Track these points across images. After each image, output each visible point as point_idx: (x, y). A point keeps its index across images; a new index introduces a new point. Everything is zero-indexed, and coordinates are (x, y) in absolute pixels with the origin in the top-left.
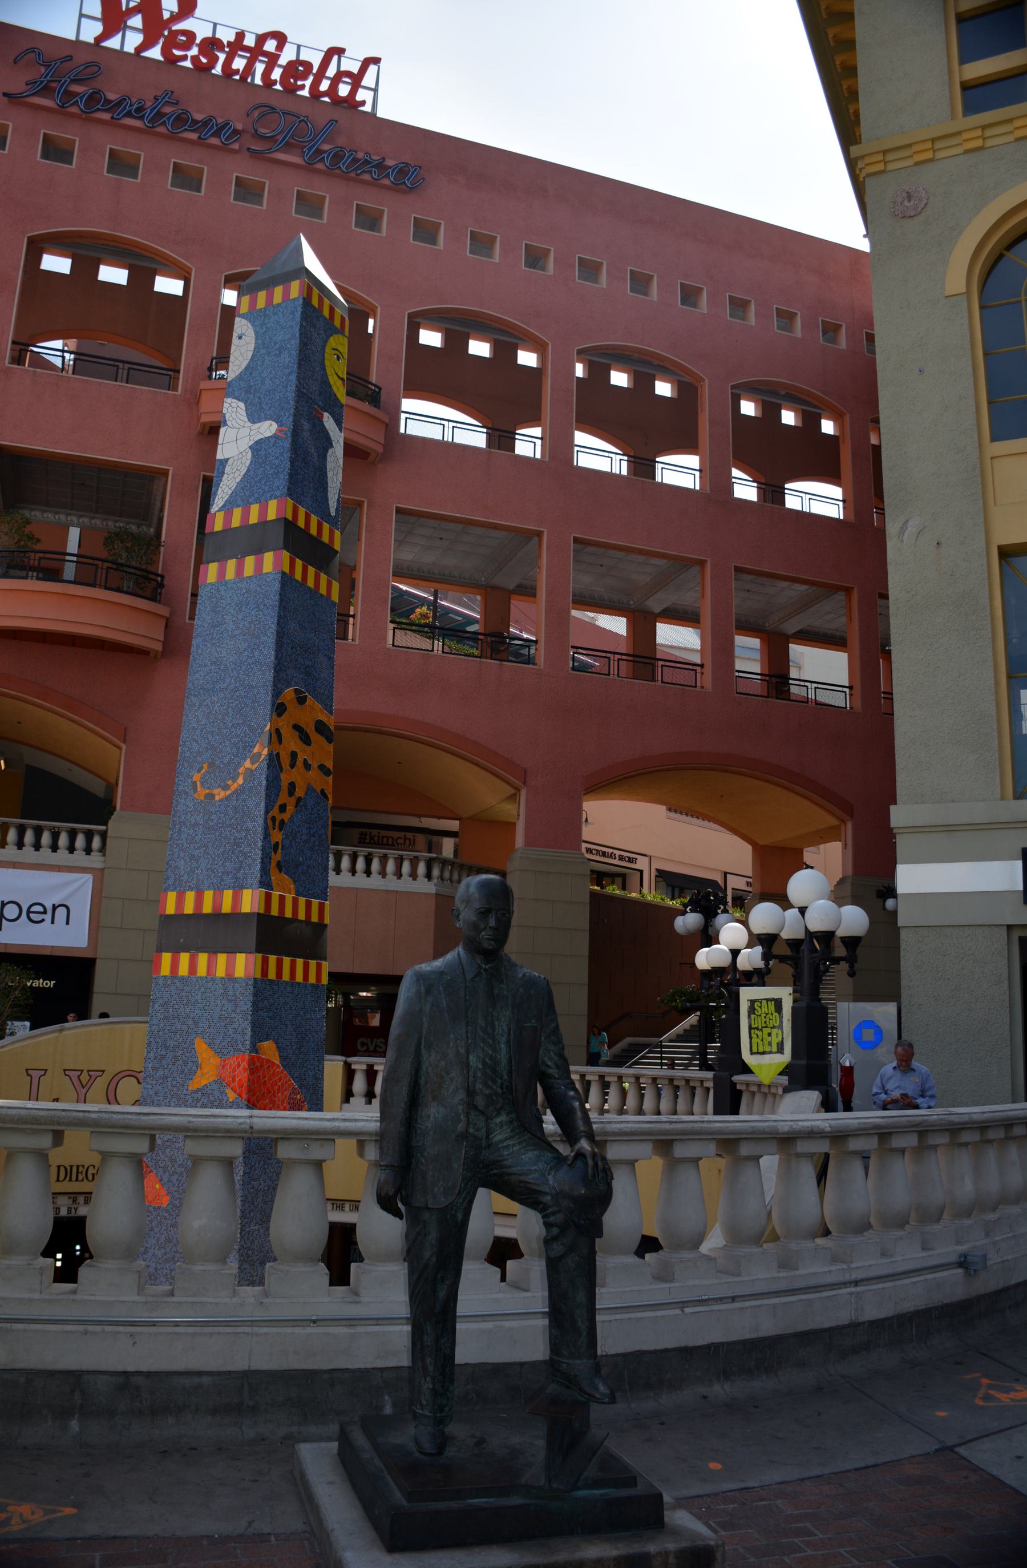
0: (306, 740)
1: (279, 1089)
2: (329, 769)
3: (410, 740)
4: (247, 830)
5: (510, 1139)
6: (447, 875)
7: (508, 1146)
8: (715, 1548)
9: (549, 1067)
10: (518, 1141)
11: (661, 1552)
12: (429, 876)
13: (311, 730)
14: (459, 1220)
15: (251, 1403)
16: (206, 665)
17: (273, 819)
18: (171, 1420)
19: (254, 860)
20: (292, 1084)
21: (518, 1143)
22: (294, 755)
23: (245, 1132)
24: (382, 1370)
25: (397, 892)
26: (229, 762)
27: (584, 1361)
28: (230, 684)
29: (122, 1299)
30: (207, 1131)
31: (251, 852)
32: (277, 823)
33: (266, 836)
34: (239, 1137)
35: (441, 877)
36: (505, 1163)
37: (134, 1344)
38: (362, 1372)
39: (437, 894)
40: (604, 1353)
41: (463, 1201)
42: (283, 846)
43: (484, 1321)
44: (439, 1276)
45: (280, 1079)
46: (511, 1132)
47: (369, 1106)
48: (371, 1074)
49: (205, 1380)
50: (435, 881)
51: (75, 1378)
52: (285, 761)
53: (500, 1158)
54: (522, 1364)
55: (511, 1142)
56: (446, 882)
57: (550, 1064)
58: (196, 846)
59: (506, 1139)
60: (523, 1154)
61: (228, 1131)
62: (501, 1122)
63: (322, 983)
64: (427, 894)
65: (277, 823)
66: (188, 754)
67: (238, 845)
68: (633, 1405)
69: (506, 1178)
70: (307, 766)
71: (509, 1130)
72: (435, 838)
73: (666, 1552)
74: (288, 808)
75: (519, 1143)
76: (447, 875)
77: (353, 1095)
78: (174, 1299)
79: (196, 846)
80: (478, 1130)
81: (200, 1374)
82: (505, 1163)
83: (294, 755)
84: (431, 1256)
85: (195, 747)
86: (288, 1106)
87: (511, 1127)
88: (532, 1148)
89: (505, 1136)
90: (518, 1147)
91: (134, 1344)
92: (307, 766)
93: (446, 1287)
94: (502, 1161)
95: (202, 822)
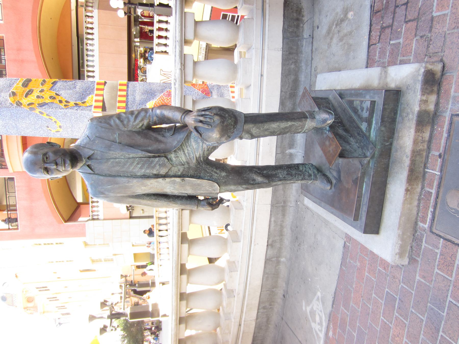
0: (31, 92)
1: (163, 101)
2: (43, 81)
3: (40, 16)
4: (71, 115)
5: (184, 152)
6: (91, 5)
7: (189, 153)
8: (426, 69)
9: (143, 125)
10: (186, 147)
11: (419, 104)
12: (92, 12)
13: (27, 89)
14: (225, 174)
15: (283, 203)
16: (7, 130)
17: (65, 106)
18: (285, 230)
19: (82, 113)
20: (162, 96)
21: (187, 148)
22: (38, 97)
23: (179, 212)
24: (276, 154)
25: (99, 24)
26: (45, 121)
27: (307, 123)
28: (12, 122)
29: (242, 247)
30: (179, 226)
31: (79, 114)
32: (67, 104)
33: (72, 108)
34: (182, 212)
35: (92, 7)
36: (198, 156)
37: (258, 244)
38: (276, 162)
39: (98, 9)
40: (282, 50)
41: (217, 173)
42: (76, 101)
43: (262, 107)
44: (252, 182)
45: (160, 100)
46: (180, 151)
47: (170, 23)
48: (160, 22)
49: (273, 219)
50: (93, 9)
51: (267, 261)
52: (41, 101)
53: (195, 158)
54: (281, 91)
55: (186, 151)
56: (94, 5)
57: (141, 125)
58: (80, 130)
59: (185, 154)
60: (193, 147)
61: (179, 218)
62: (175, 157)
63: (126, 83)
64: (98, 13)
65: (67, 104)
66: (45, 134)
67: (77, 118)
68: (305, 36)
69: (206, 155)
70: (42, 91)
71: (180, 152)
72: (79, 4)
73: (420, 101)
74: (60, 99)
75: (187, 147)
76: (91, 5)
77: (168, 4)
78: (243, 230)
79: (80, 130)
80: (179, 170)
81: (270, 221)
82: (198, 156)
83: (38, 97)
84: (242, 187)
85: (42, 132)
86: (170, 97)
87: (178, 151)
88: (190, 141)
89: (182, 154)
90: (189, 148)
91: (258, 244)
92: (42, 91)
93: (257, 178)
94: (196, 157)
95: (71, 129)
